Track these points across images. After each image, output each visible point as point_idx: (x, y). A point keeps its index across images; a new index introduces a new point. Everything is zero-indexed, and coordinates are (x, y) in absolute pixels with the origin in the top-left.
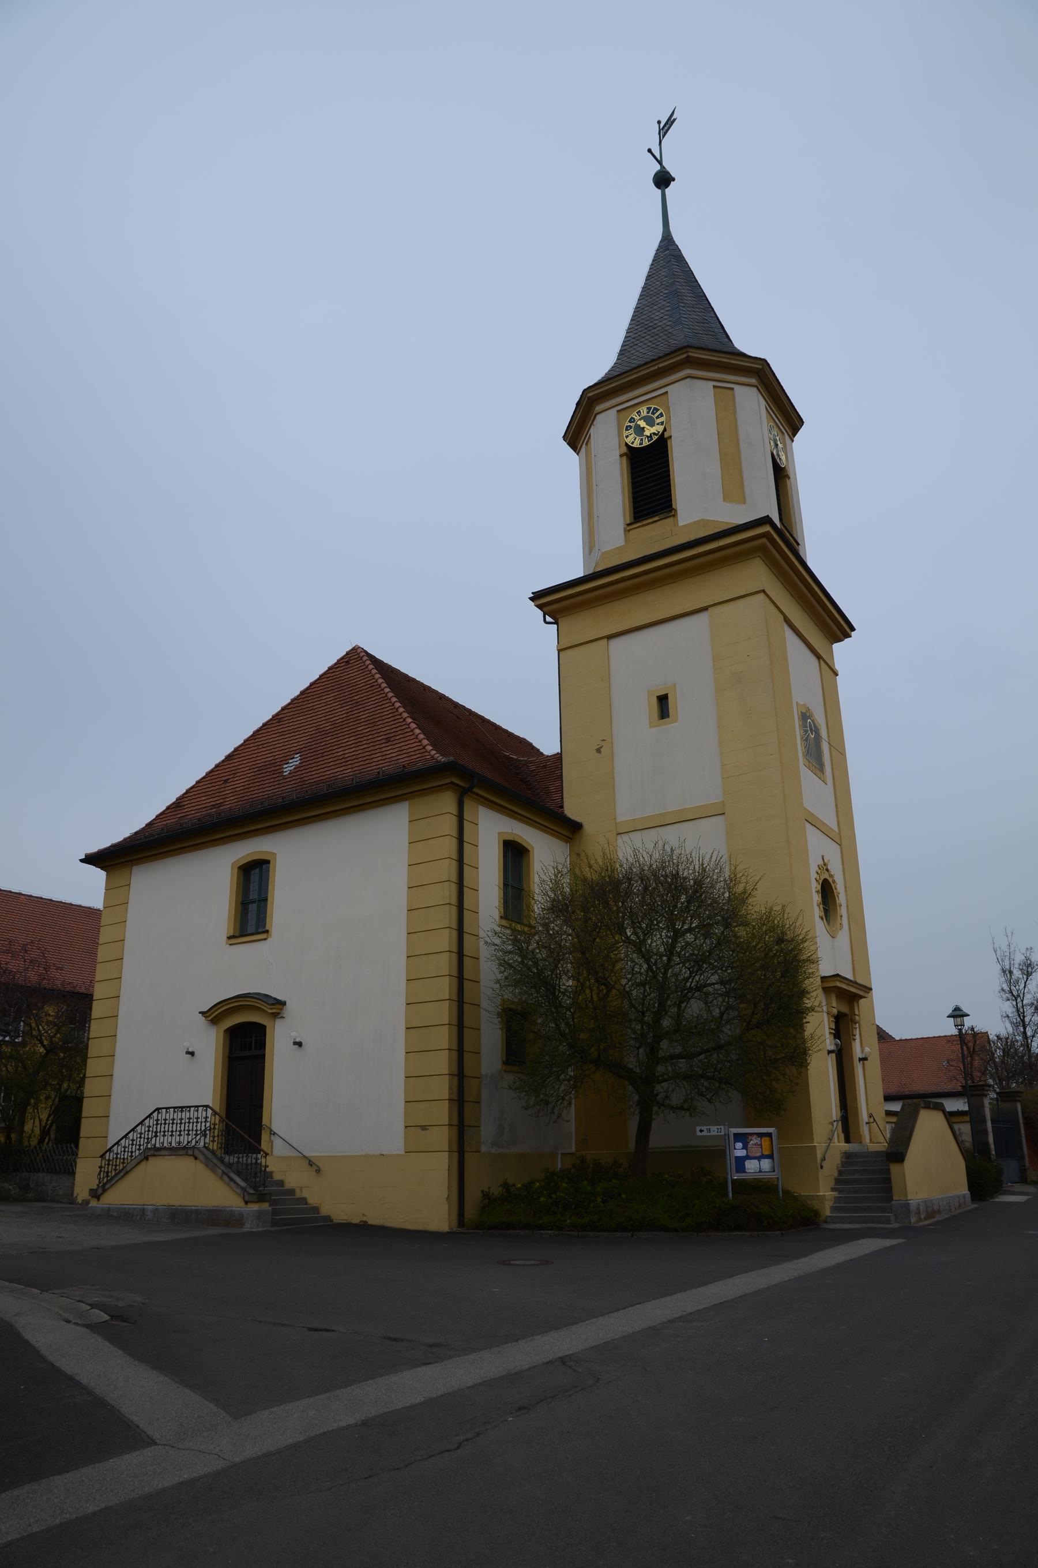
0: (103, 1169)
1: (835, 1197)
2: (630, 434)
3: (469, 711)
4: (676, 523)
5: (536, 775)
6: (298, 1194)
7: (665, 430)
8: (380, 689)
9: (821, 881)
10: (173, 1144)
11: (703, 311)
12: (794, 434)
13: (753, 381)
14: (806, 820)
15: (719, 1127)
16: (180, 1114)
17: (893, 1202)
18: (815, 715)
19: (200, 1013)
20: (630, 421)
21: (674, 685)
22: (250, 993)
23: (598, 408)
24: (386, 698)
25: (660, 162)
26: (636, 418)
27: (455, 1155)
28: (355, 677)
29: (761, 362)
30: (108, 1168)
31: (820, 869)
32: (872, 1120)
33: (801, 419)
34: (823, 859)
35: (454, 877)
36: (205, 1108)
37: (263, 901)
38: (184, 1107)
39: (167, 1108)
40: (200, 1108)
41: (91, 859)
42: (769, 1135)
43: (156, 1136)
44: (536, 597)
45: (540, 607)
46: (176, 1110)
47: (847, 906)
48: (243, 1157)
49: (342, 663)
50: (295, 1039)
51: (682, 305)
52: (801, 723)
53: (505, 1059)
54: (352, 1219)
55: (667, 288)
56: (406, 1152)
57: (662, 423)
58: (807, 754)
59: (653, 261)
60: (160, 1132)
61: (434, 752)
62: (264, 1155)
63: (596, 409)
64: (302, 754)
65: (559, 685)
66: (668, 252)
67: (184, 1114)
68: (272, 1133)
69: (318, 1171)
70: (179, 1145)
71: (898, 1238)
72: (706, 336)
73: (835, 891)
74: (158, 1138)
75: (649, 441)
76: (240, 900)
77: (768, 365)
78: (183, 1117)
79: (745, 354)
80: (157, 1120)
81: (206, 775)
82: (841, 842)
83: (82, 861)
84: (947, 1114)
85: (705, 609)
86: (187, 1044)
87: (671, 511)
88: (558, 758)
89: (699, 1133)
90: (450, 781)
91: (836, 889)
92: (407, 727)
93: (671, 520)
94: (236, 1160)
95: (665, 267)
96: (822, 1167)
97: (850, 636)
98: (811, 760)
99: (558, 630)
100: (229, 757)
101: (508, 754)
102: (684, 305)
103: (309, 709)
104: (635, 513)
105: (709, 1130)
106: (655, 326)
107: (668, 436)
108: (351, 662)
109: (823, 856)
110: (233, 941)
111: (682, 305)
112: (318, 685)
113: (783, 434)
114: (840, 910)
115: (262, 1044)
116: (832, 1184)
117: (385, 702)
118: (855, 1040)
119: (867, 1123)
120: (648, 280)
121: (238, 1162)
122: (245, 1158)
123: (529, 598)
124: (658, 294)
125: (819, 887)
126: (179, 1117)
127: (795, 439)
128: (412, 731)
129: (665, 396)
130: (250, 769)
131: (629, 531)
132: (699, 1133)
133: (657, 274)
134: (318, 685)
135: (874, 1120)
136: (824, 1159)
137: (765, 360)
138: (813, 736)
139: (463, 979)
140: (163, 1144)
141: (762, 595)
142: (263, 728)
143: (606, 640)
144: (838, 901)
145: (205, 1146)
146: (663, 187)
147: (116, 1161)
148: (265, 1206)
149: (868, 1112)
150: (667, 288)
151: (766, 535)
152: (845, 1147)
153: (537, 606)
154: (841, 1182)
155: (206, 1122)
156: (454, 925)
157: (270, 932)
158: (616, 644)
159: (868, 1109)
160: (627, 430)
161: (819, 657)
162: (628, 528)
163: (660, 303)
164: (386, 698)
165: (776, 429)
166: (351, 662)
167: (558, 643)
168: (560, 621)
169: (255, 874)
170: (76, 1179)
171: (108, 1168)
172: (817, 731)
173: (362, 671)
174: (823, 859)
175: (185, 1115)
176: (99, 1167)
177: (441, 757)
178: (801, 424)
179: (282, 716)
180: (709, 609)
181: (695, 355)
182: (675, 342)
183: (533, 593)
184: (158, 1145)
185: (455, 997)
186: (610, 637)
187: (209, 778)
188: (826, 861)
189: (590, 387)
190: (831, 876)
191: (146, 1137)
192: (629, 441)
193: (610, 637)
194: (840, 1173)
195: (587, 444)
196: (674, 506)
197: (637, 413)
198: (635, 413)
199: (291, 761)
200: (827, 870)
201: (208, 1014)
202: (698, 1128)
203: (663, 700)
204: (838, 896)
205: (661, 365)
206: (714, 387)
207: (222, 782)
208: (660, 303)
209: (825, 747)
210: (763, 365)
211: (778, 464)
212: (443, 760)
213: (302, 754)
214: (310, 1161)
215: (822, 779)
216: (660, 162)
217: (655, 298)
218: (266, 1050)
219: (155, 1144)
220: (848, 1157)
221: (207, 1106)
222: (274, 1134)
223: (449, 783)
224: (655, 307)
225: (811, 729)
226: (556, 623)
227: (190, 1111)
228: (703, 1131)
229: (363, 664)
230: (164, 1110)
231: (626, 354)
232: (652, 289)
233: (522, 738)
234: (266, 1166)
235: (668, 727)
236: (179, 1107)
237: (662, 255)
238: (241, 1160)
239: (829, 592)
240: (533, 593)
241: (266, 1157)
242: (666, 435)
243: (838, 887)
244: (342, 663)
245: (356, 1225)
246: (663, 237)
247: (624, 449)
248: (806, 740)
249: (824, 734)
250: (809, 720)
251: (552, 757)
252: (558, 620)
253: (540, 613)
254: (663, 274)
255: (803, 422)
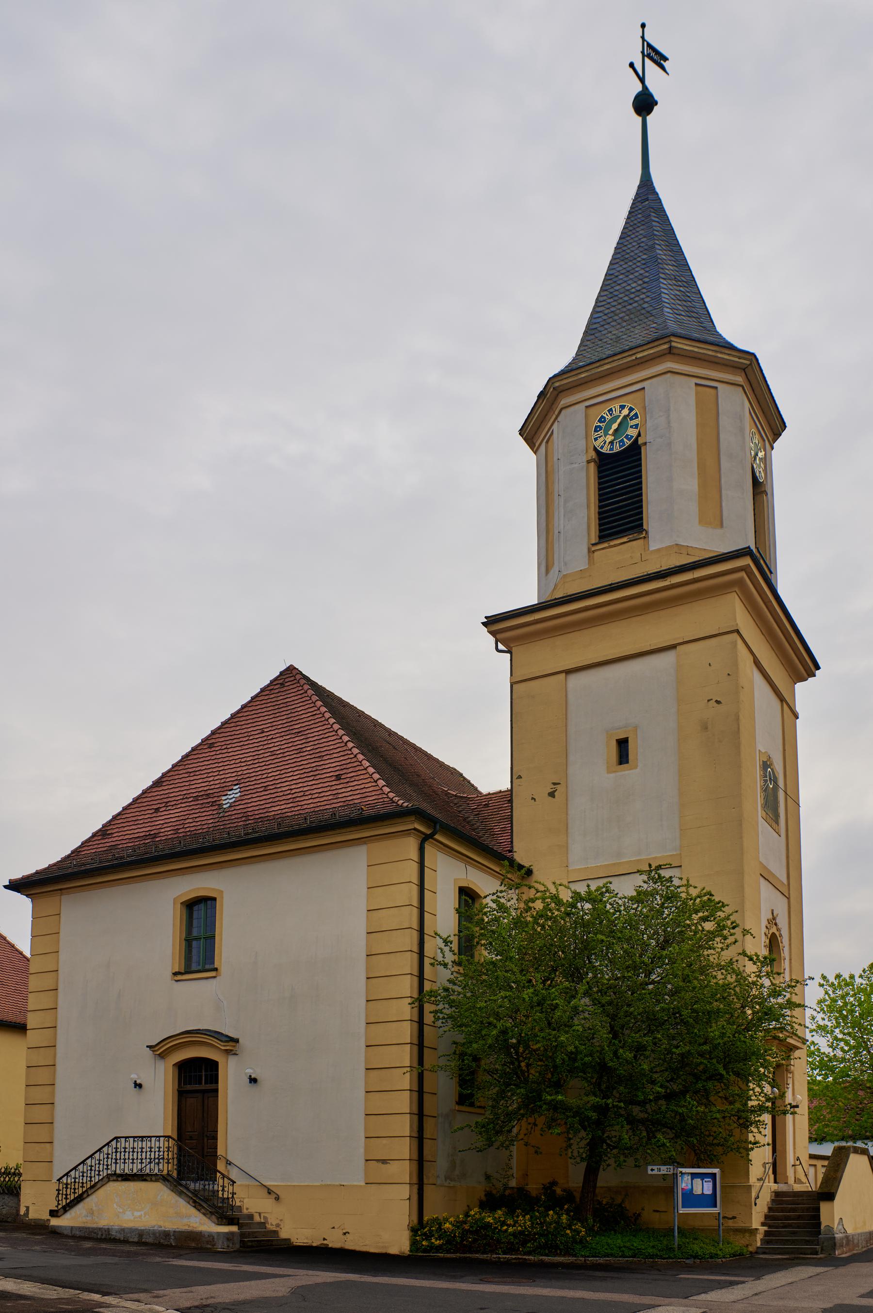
0: (61, 1192)
1: (765, 1231)
2: (600, 437)
3: (401, 738)
4: (646, 547)
5: (478, 814)
6: (257, 1219)
7: (639, 435)
8: (323, 719)
9: (769, 935)
10: (126, 1171)
11: (687, 285)
12: (775, 441)
13: (739, 379)
14: (761, 875)
15: (668, 1167)
16: (140, 1143)
17: (820, 1236)
18: (775, 763)
19: (147, 1047)
20: (600, 421)
21: (636, 728)
22: (199, 1030)
23: (564, 402)
24: (331, 730)
25: (642, 80)
26: (607, 417)
27: (416, 1187)
28: (293, 703)
29: (750, 358)
30: (66, 1191)
31: (769, 923)
32: (798, 1163)
33: (784, 423)
34: (773, 914)
35: (415, 925)
36: (167, 1139)
37: (210, 939)
38: (145, 1137)
39: (126, 1138)
40: (152, 1138)
41: (15, 886)
42: (714, 1175)
43: (116, 1163)
44: (490, 622)
45: (493, 633)
46: (136, 1139)
47: (790, 960)
48: (209, 1184)
49: (275, 685)
50: (250, 1076)
51: (663, 276)
52: (762, 772)
53: (457, 1100)
54: (313, 1242)
55: (645, 252)
56: (366, 1184)
57: (636, 426)
58: (765, 806)
59: (630, 213)
60: (120, 1159)
61: (391, 795)
62: (231, 1183)
63: (562, 402)
64: (242, 785)
65: (511, 721)
66: (647, 202)
67: (144, 1143)
68: (228, 1162)
69: (277, 1198)
70: (141, 1172)
71: (825, 1266)
72: (689, 318)
73: (780, 944)
74: (118, 1165)
75: (620, 447)
76: (184, 936)
77: (757, 360)
78: (144, 1146)
79: (732, 345)
80: (116, 1148)
81: (133, 801)
82: (789, 894)
83: (6, 887)
84: (870, 1157)
85: (673, 647)
86: (134, 1076)
87: (641, 532)
88: (507, 798)
89: (650, 1172)
90: (413, 828)
91: (782, 943)
92: (360, 764)
93: (640, 542)
94: (202, 1186)
95: (643, 223)
96: (756, 1204)
97: (815, 676)
98: (769, 813)
99: (511, 660)
100: (157, 783)
101: (446, 789)
102: (665, 277)
103: (243, 735)
104: (600, 531)
105: (659, 1170)
106: (631, 301)
107: (642, 442)
108: (286, 684)
109: (773, 910)
110: (179, 977)
111: (663, 276)
112: (250, 709)
113: (764, 441)
114: (784, 963)
115: (214, 1078)
116: (762, 1219)
117: (331, 734)
118: (788, 1088)
119: (793, 1166)
120: (624, 238)
121: (204, 1190)
122: (211, 1186)
123: (482, 623)
124: (635, 259)
125: (768, 941)
126: (140, 1146)
127: (775, 445)
128: (366, 769)
129: (643, 391)
130: (183, 799)
131: (593, 552)
132: (650, 1172)
133: (634, 231)
134: (250, 709)
135: (801, 1163)
136: (758, 1197)
137: (753, 355)
138: (771, 786)
139: (423, 1024)
140: (132, 1170)
141: (735, 635)
142: (193, 753)
143: (564, 675)
144: (782, 955)
145: (168, 1174)
146: (644, 113)
147: (74, 1185)
148: (234, 1229)
149: (794, 1156)
150: (645, 252)
151: (745, 569)
152: (775, 1187)
153: (490, 632)
154: (769, 1219)
155: (159, 1151)
156: (416, 972)
157: (219, 971)
158: (575, 680)
159: (795, 1153)
160: (596, 431)
161: (782, 699)
162: (593, 549)
163: (637, 271)
164: (331, 730)
165: (757, 436)
166: (286, 684)
167: (511, 675)
168: (514, 650)
169: (200, 911)
170: (21, 1200)
171: (66, 1191)
172: (775, 781)
173: (300, 696)
174: (773, 914)
175: (146, 1144)
176: (57, 1190)
177: (402, 801)
178: (783, 428)
179: (213, 741)
180: (678, 647)
181: (679, 346)
182: (655, 325)
183: (486, 617)
184: (118, 1172)
185: (416, 1041)
186: (568, 672)
187: (136, 805)
188: (775, 915)
189: (555, 376)
190: (778, 930)
191: (105, 1163)
192: (598, 444)
193: (568, 672)
194: (770, 1209)
195: (547, 442)
196: (645, 527)
197: (609, 411)
198: (606, 411)
199: (229, 793)
200: (776, 924)
201: (156, 1049)
202: (650, 1168)
203: (623, 744)
204: (783, 950)
205: (639, 356)
206: (696, 384)
207: (153, 811)
208: (637, 271)
209: (781, 795)
210: (751, 361)
211: (757, 477)
212: (405, 804)
213: (242, 785)
214: (269, 1189)
215: (777, 831)
216: (642, 80)
217: (630, 264)
218: (219, 1084)
219: (115, 1171)
220: (778, 1196)
221: (169, 1137)
222: (230, 1164)
223: (413, 829)
224: (631, 276)
225: (770, 779)
226: (509, 652)
227: (159, 1140)
228: (654, 1170)
229: (300, 688)
230: (123, 1140)
231: (596, 335)
232: (628, 251)
233: (452, 768)
234: (233, 1193)
235: (629, 775)
236: (140, 1137)
237: (640, 207)
238: (207, 1187)
239: (800, 629)
240: (486, 617)
241: (233, 1185)
242: (640, 441)
243: (783, 940)
244: (275, 685)
245: (316, 1247)
246: (641, 181)
247: (593, 454)
248: (765, 791)
249: (781, 783)
250: (769, 769)
251: (495, 796)
252: (511, 648)
253: (492, 640)
254: (641, 232)
255: (785, 427)
